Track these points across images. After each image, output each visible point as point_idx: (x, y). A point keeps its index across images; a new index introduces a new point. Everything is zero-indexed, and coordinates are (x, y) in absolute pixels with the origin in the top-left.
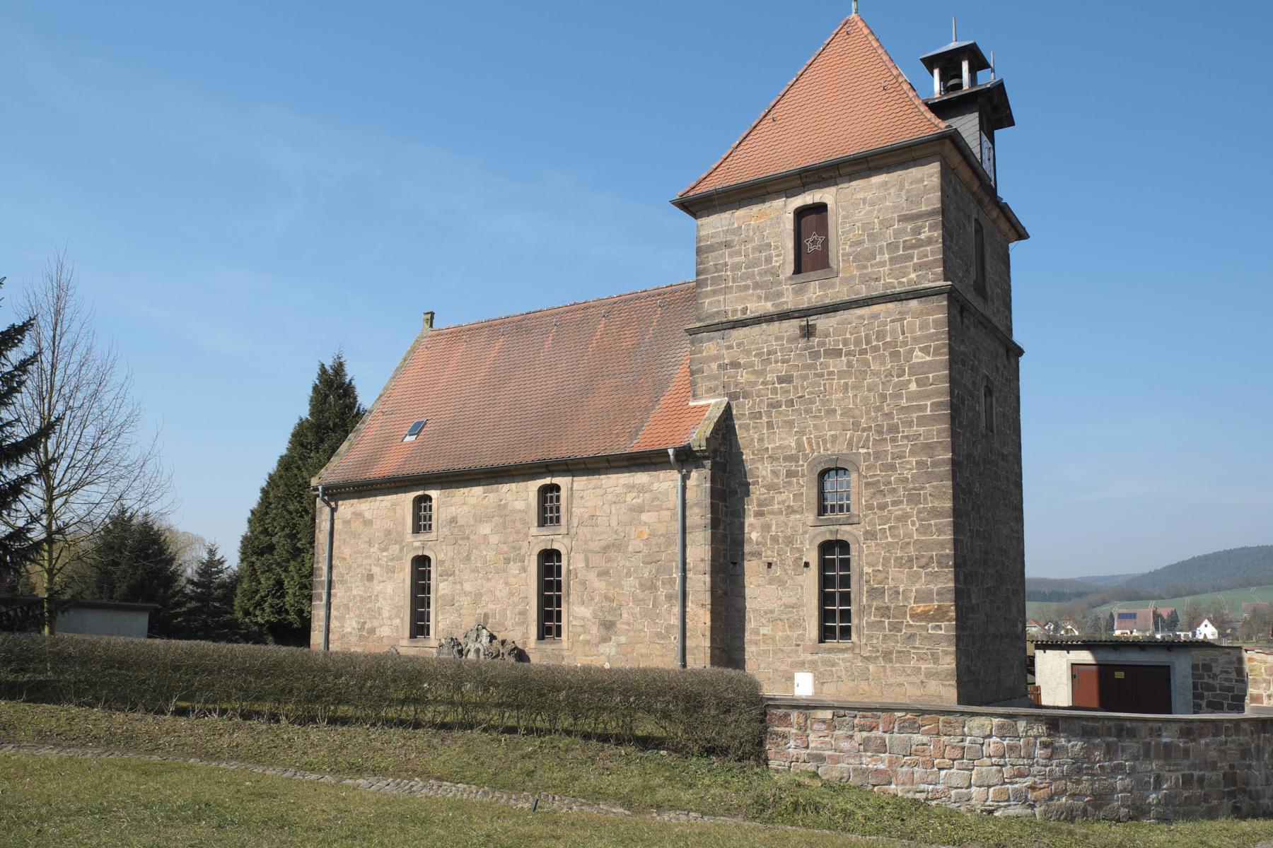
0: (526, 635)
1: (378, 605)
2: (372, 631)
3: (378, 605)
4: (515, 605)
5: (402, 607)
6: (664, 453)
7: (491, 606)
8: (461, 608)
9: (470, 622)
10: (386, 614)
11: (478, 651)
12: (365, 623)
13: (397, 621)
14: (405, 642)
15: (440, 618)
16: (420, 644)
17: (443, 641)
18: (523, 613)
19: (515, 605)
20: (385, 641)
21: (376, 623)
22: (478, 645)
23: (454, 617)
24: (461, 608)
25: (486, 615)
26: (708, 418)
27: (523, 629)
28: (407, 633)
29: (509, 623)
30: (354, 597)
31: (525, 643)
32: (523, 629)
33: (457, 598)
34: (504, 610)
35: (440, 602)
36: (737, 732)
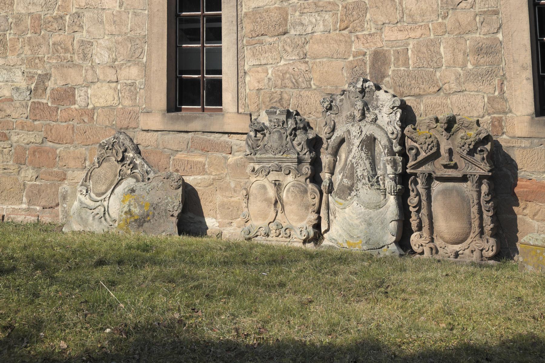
0: (499, 104)
1: (83, 35)
2: (66, 95)
3: (83, 35)
4: (462, 32)
5: (145, 39)
6: (377, 126)
7: (391, 34)
8: (306, 39)
9: (334, 73)
10: (101, 55)
11: (369, 143)
12: (47, 76)
13: (133, 73)
14: (156, 121)
15: (248, 63)
16: (196, 125)
17: (264, 119)
18: (489, 50)
19: (462, 32)
20: (100, 119)
21: (75, 77)
22: (369, 129)
23: (288, 61)
24: (306, 39)
25: (379, 58)
26: (325, 167)
27: (490, 89)
28: (160, 97)
29: (447, 76)
30: (19, 20)
31: (498, 124)
32: (490, 89)
33: (294, 16)
34: (433, 45)
35: (248, 26)
36: (372, 45)
